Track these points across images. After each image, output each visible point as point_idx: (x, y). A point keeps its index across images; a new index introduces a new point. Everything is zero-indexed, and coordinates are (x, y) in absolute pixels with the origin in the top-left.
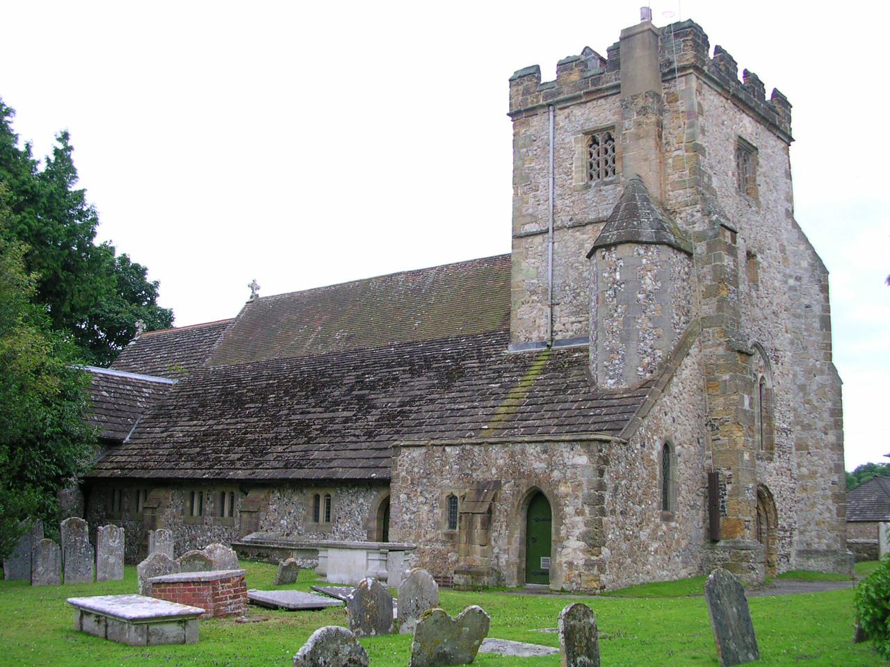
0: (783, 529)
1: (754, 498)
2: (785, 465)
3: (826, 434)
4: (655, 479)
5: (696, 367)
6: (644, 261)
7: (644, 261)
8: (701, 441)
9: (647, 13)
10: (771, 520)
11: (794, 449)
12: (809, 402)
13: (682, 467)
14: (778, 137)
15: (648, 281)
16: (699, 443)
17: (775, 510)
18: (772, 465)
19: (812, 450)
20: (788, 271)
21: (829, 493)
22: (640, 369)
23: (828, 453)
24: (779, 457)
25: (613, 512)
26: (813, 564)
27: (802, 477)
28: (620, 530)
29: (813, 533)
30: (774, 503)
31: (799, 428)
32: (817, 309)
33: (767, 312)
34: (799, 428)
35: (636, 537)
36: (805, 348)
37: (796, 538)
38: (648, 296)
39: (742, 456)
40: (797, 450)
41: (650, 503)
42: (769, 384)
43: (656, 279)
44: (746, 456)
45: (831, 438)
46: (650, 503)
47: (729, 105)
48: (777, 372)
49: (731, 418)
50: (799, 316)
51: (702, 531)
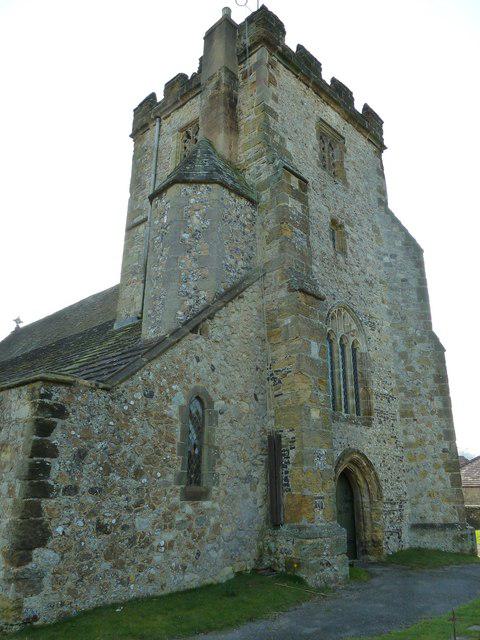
0: (390, 502)
1: (329, 467)
2: (388, 432)
3: (432, 400)
4: (172, 441)
5: (255, 312)
6: (192, 201)
7: (192, 201)
8: (259, 397)
9: (227, 11)
10: (374, 493)
11: (398, 417)
12: (410, 369)
13: (226, 428)
14: (369, 140)
15: (196, 220)
16: (256, 399)
17: (377, 480)
18: (371, 430)
19: (419, 417)
20: (382, 250)
21: (440, 461)
22: (180, 313)
23: (436, 420)
24: (380, 423)
25: (72, 490)
26: (428, 541)
27: (409, 445)
28: (88, 516)
29: (427, 506)
30: (375, 474)
31: (403, 394)
32: (414, 283)
33: (361, 279)
34: (403, 394)
35: (125, 528)
36: (403, 318)
37: (407, 511)
38: (193, 236)
39: (308, 413)
40: (402, 416)
41: (159, 475)
42: (362, 348)
43: (204, 217)
44: (315, 414)
45: (437, 404)
46: (159, 475)
47: (310, 92)
48: (374, 338)
49: (292, 368)
50: (396, 289)
51: (262, 512)
